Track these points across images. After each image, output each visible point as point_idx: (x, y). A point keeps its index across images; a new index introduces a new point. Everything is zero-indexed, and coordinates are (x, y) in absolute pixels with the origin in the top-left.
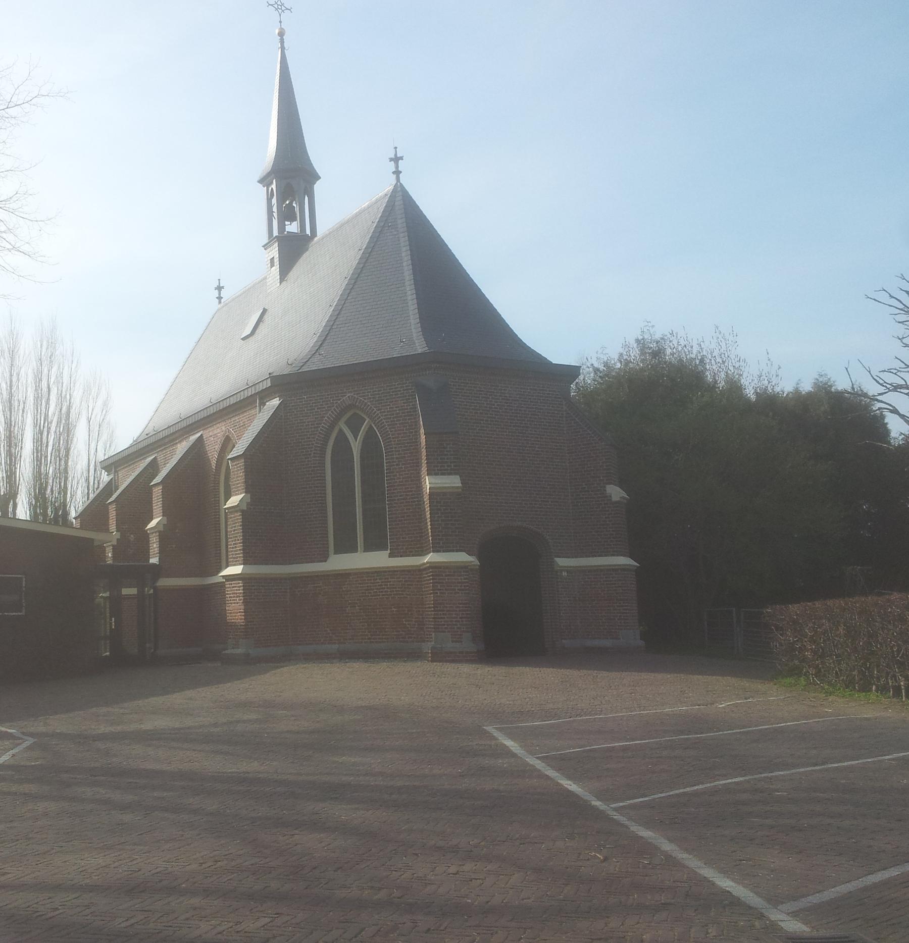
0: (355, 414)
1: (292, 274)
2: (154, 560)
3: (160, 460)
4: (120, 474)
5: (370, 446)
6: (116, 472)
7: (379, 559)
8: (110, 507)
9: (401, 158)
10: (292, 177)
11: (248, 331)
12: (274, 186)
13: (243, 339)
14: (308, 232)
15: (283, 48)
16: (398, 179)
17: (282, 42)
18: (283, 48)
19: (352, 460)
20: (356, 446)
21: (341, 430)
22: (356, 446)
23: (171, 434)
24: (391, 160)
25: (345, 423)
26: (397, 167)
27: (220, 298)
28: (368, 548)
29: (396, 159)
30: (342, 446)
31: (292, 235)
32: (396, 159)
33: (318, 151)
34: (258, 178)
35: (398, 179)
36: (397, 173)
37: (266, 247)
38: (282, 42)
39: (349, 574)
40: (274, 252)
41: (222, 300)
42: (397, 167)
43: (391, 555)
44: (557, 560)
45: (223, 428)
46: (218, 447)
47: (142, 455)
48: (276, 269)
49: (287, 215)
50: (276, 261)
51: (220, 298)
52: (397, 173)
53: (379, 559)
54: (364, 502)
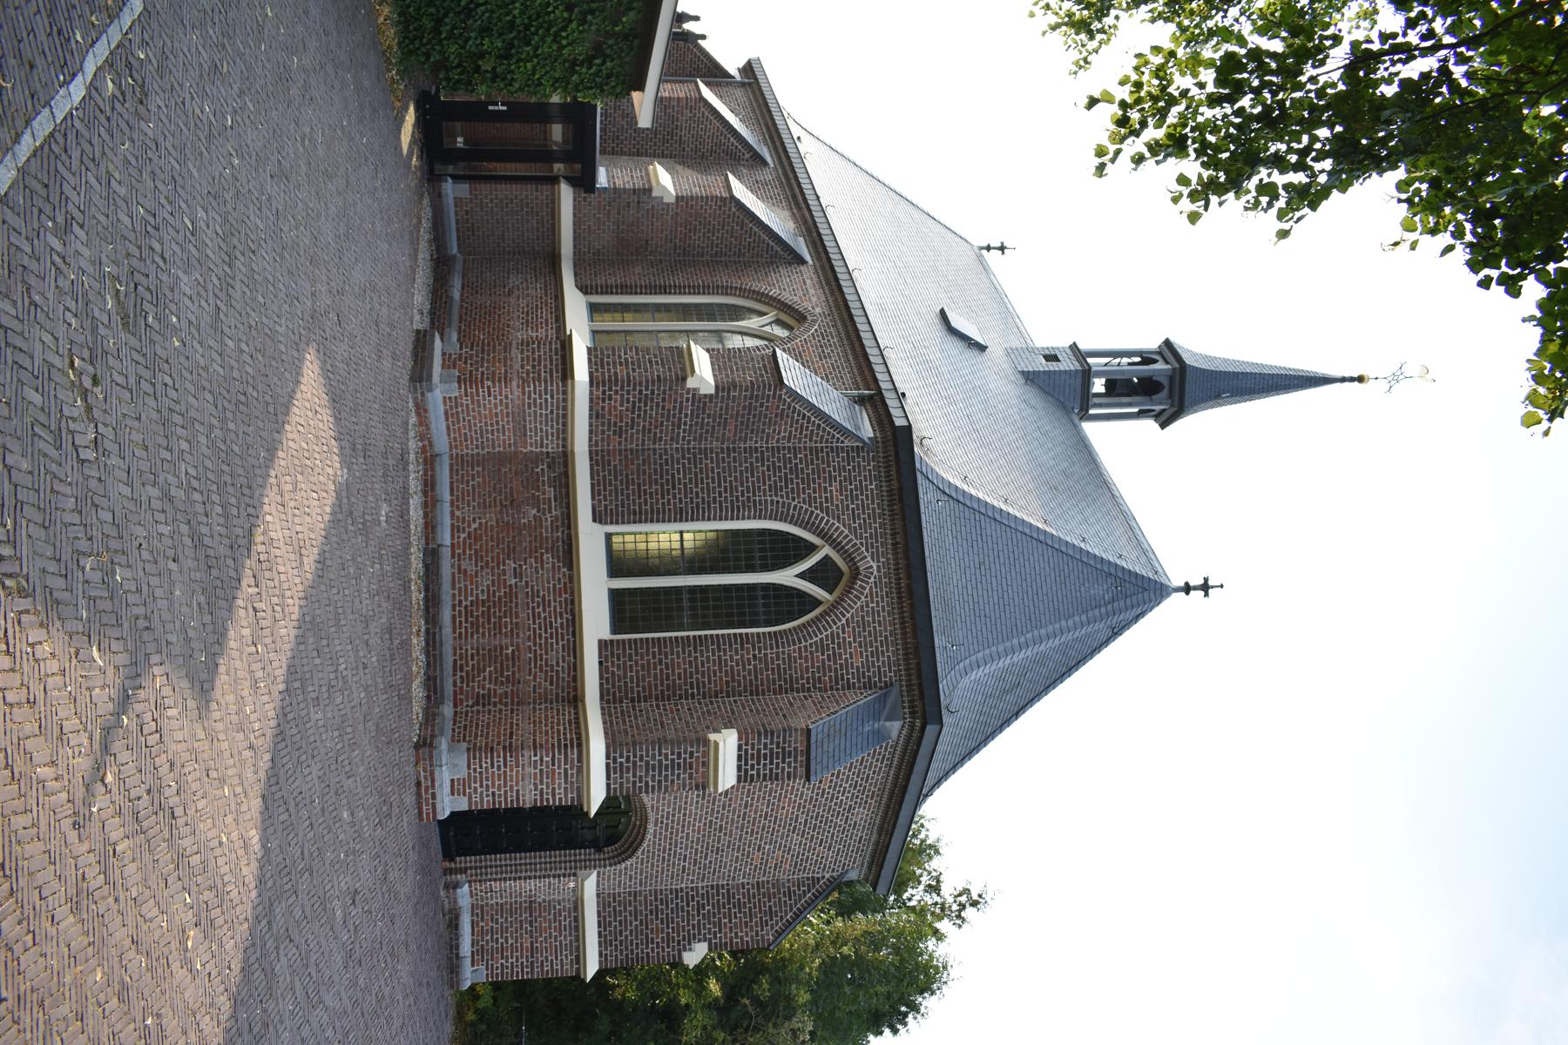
0: (841, 573)
1: (1032, 395)
2: (602, 178)
3: (767, 175)
4: (739, 92)
5: (789, 603)
6: (743, 84)
7: (596, 623)
8: (691, 86)
9: (1206, 595)
10: (1167, 386)
11: (957, 322)
12: (1160, 366)
13: (942, 312)
14: (1091, 412)
15: (1343, 380)
16: (1178, 590)
17: (1352, 379)
18: (1343, 380)
19: (766, 568)
20: (787, 577)
21: (811, 549)
22: (787, 577)
23: (805, 200)
24: (1206, 580)
25: (827, 557)
26: (1195, 588)
27: (988, 248)
28: (616, 597)
29: (1205, 587)
30: (784, 550)
31: (1087, 384)
32: (1205, 587)
33: (1204, 425)
34: (1172, 339)
35: (1178, 590)
36: (1187, 589)
37: (1074, 347)
38: (1352, 379)
39: (571, 568)
40: (1068, 364)
41: (984, 252)
42: (1195, 588)
43: (603, 645)
44: (594, 876)
45: (818, 310)
46: (786, 297)
47: (771, 138)
48: (1041, 365)
49: (1117, 387)
50: (1053, 366)
51: (988, 248)
52: (1187, 589)
53: (596, 623)
54: (693, 590)
